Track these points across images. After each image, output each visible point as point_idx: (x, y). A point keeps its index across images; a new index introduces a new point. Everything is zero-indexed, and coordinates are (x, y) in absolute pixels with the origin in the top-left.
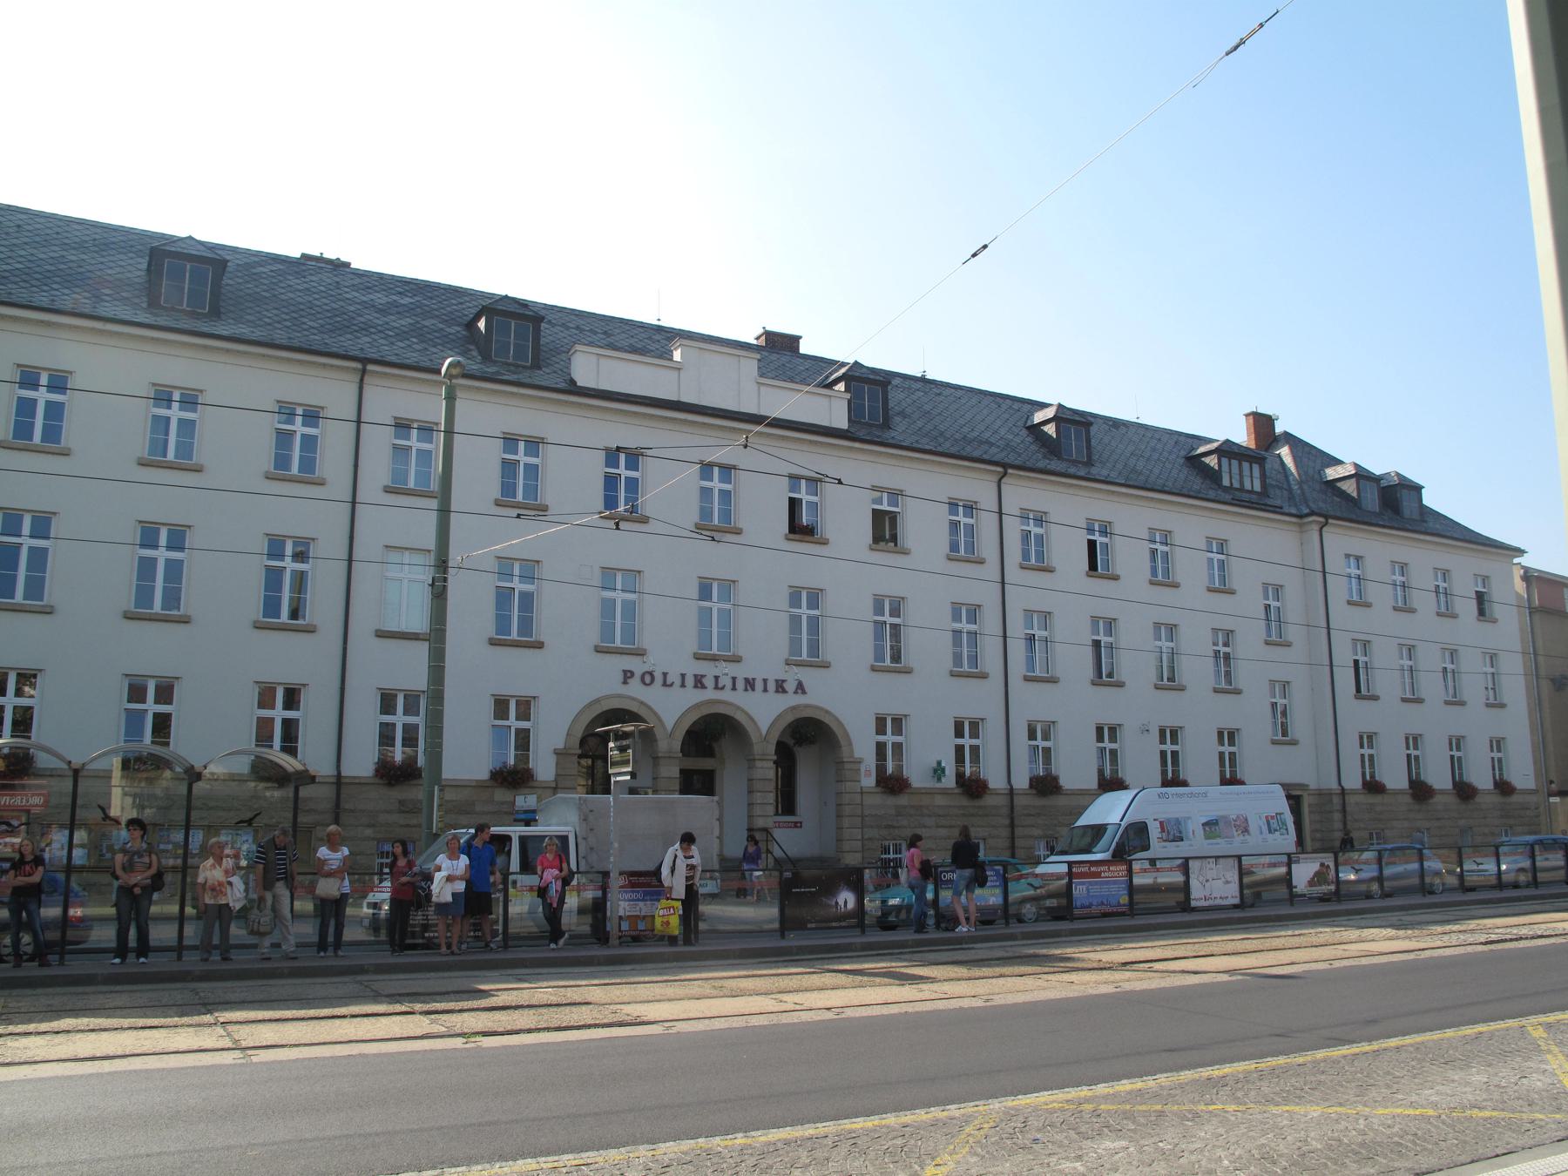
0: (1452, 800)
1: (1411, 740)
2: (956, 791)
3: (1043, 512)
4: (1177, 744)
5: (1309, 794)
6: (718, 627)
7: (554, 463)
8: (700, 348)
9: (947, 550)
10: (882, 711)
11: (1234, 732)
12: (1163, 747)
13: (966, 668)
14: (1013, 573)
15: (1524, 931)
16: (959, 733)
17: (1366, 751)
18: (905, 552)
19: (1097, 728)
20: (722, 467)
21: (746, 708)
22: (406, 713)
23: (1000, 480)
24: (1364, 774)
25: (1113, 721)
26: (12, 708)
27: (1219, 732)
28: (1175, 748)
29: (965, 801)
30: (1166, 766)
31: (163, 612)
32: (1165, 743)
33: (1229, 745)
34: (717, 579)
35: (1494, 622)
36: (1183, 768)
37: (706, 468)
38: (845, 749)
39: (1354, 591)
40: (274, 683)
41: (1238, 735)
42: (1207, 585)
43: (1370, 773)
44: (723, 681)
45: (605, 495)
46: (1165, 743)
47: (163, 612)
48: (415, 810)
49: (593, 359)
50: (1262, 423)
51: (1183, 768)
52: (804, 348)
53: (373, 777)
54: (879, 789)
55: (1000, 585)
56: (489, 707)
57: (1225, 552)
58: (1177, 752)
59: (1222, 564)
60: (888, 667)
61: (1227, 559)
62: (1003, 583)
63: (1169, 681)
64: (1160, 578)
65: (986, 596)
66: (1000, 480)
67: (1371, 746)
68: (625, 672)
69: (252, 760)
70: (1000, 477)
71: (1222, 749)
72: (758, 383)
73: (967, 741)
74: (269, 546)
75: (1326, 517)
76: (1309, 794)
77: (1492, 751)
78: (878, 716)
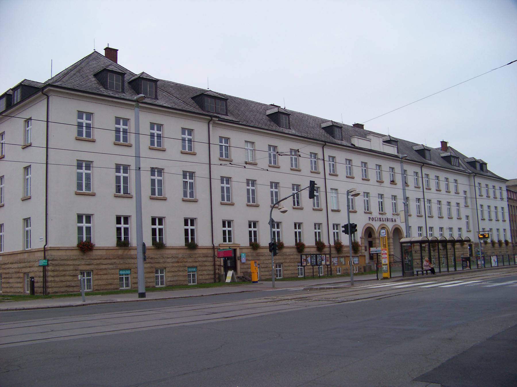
0: (491, 245)
1: (419, 228)
2: (153, 248)
3: (228, 138)
4: (256, 228)
5: (240, 248)
6: (252, 195)
7: (97, 122)
8: (373, 136)
9: (149, 145)
10: (119, 214)
11: (194, 220)
12: (250, 229)
13: (188, 198)
14: (327, 176)
15: (171, 322)
16: (186, 224)
17: (317, 231)
18: (396, 184)
19: (152, 219)
20: (87, 113)
21: (388, 226)
22: (159, 225)
23: (323, 147)
24: (316, 239)
25: (161, 215)
26: (123, 228)
27: (223, 222)
28: (230, 229)
29: (188, 252)
30: (188, 236)
31: (190, 198)
32: (188, 225)
33: (254, 228)
34: (251, 180)
35: (396, 184)
36: (233, 236)
37: (183, 130)
38: (403, 235)
39: (378, 177)
40: (230, 220)
41: (232, 223)
42: (114, 141)
43: (337, 239)
44: (384, 219)
45: (151, 140)
46: (188, 225)
47: (190, 198)
48: (283, 255)
49: (357, 139)
50: (444, 144)
51: (233, 236)
52: (365, 128)
53: (116, 246)
54: (186, 247)
55: (324, 179)
56: (115, 220)
57: (406, 174)
58: (231, 231)
59: (315, 162)
60: (157, 197)
61: (335, 164)
62: (210, 164)
63: (276, 204)
64: (187, 150)
65: (201, 171)
66: (323, 147)
67: (299, 228)
68: (369, 218)
69: (502, 241)
70: (323, 146)
71: (296, 230)
72: (383, 144)
73: (157, 227)
74: (77, 164)
75: (476, 174)
76: (240, 248)
77: (419, 231)
78: (117, 216)
